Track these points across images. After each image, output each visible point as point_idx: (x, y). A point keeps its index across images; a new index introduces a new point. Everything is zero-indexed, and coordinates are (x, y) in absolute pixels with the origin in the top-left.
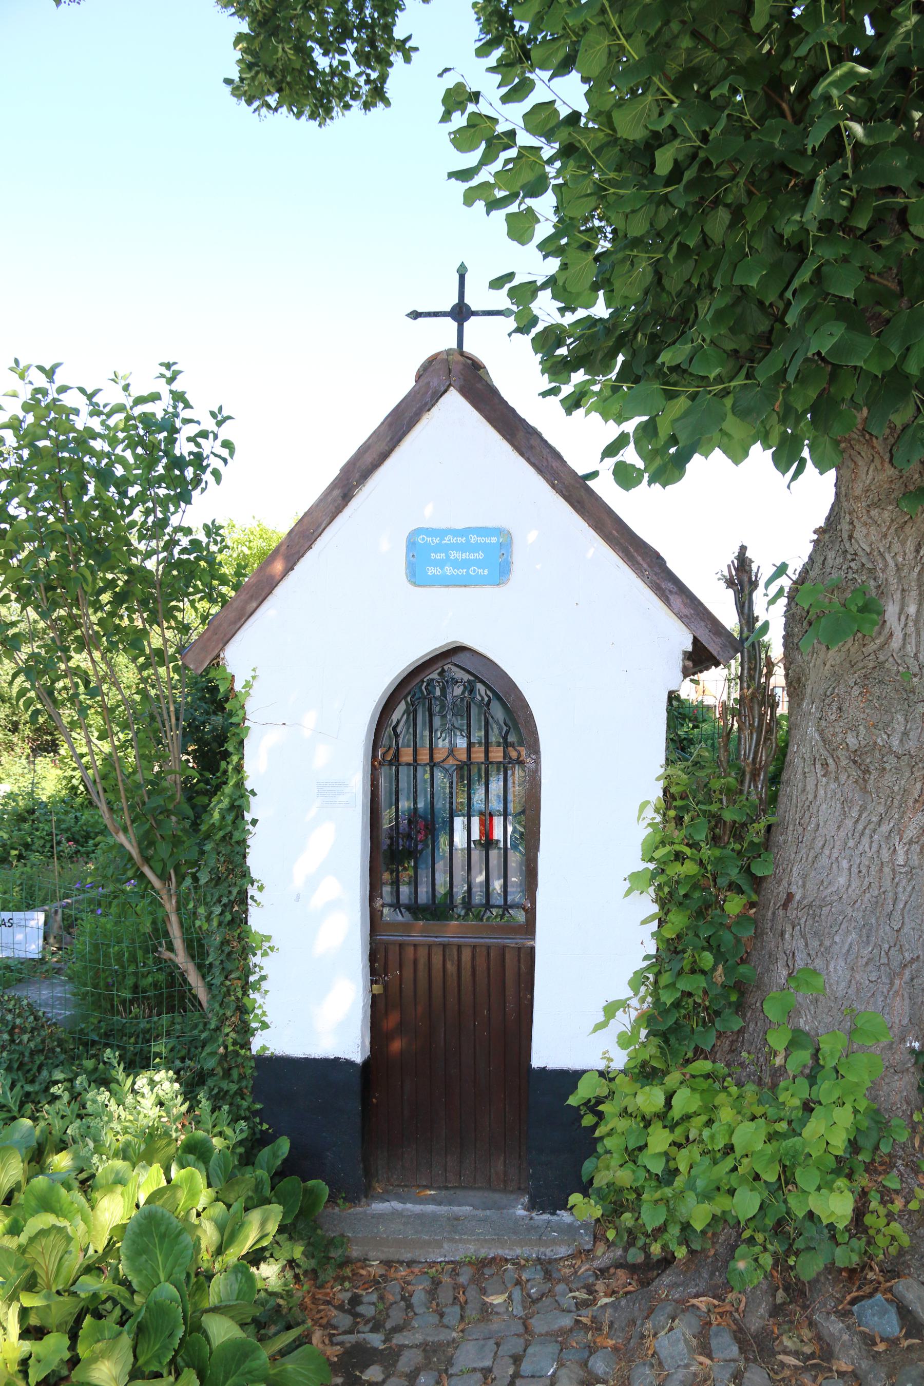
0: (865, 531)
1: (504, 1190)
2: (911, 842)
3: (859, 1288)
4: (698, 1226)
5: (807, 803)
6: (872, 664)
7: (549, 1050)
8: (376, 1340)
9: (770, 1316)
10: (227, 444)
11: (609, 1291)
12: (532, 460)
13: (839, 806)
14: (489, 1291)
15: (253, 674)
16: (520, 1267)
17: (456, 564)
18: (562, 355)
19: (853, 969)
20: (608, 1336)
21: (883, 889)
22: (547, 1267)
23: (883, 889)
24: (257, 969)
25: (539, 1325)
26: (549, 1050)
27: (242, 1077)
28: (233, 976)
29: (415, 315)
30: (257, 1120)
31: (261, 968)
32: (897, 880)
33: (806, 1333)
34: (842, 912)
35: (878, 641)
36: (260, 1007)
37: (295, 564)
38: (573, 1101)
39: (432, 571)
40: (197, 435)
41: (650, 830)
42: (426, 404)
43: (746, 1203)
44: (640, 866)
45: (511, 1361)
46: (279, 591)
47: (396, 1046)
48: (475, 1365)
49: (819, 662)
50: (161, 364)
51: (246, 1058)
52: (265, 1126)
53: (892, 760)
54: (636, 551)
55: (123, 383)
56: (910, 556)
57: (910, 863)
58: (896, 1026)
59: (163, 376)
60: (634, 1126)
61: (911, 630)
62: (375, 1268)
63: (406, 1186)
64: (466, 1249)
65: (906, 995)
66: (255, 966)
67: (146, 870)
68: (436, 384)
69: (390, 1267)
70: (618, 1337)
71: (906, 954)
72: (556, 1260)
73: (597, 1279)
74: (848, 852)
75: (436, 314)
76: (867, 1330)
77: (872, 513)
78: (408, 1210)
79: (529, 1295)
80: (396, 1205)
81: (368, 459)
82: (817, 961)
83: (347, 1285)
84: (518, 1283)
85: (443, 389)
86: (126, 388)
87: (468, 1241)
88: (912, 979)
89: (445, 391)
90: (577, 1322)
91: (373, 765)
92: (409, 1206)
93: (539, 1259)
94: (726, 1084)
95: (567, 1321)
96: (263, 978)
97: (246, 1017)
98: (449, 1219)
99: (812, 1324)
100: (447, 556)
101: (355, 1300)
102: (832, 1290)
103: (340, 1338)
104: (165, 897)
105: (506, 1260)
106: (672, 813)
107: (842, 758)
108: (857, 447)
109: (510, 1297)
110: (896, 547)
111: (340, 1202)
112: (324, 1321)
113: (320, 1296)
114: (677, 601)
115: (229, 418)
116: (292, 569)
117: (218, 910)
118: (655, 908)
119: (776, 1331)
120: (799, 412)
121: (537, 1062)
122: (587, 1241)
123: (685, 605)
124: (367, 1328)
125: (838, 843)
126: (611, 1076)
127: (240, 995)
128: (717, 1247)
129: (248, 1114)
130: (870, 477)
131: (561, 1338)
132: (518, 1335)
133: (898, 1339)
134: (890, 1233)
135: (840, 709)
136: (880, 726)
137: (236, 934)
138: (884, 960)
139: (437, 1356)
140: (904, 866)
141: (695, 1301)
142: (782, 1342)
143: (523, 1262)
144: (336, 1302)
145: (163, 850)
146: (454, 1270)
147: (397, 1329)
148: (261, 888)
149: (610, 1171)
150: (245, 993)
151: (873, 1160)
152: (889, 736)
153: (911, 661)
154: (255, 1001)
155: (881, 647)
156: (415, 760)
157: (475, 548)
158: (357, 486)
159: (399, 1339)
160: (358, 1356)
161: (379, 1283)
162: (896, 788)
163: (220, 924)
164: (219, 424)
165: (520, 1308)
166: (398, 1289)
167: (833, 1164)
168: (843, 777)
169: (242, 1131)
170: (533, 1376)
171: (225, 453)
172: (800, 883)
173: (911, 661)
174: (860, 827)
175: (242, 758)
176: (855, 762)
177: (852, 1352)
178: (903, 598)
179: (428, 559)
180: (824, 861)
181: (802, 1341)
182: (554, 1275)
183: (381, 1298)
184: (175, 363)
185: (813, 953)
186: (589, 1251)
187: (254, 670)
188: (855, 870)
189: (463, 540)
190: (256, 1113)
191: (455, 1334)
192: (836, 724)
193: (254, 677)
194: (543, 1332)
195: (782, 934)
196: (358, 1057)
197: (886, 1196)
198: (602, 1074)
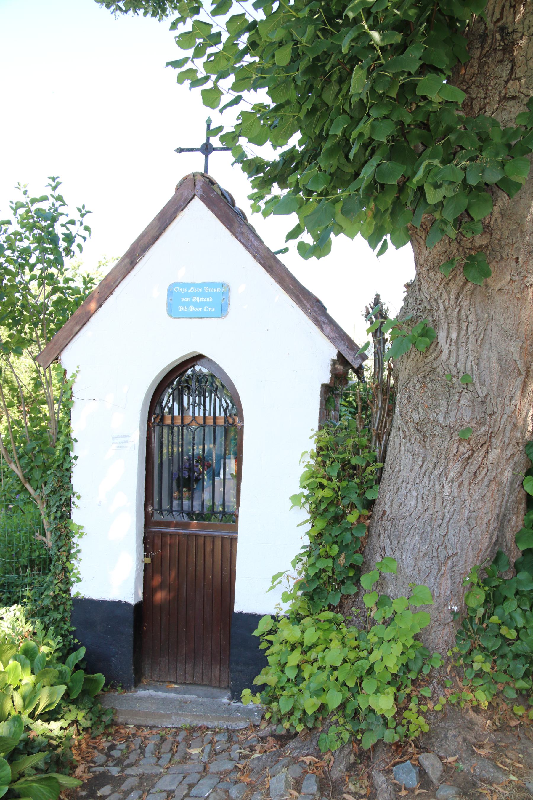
0: (427, 286)
1: (219, 687)
2: (452, 481)
3: (401, 757)
4: (310, 712)
5: (395, 455)
6: (428, 369)
7: (243, 603)
8: (115, 771)
9: (347, 770)
10: (87, 229)
11: (263, 750)
12: (243, 241)
13: (411, 457)
14: (192, 746)
15: (77, 369)
16: (215, 733)
17: (196, 305)
18: (264, 175)
19: (416, 558)
20: (248, 776)
21: (436, 510)
22: (231, 734)
23: (436, 510)
24: (75, 546)
25: (213, 768)
26: (243, 603)
27: (65, 610)
28: (62, 550)
29: (180, 150)
30: (72, 637)
31: (78, 545)
32: (444, 504)
33: (366, 782)
34: (411, 523)
35: (433, 355)
36: (77, 568)
37: (102, 303)
38: (256, 633)
39: (182, 309)
40: (68, 223)
41: (306, 469)
42: (180, 206)
43: (334, 700)
44: (298, 490)
45: (187, 787)
46: (92, 319)
47: (160, 596)
48: (166, 789)
49: (404, 367)
50: (49, 178)
51: (69, 599)
52: (76, 641)
53: (438, 429)
54: (304, 297)
55: (23, 189)
56: (453, 302)
57: (453, 494)
58: (442, 596)
59: (50, 185)
60: (284, 649)
61: (453, 348)
62: (131, 729)
63: (162, 681)
64: (185, 721)
65: (449, 577)
66: (74, 543)
67: (27, 486)
68: (186, 194)
69: (139, 729)
70: (254, 777)
71: (449, 551)
72: (238, 730)
73: (259, 743)
74: (416, 486)
75: (192, 150)
76: (398, 782)
77: (430, 274)
78: (158, 695)
79: (215, 750)
80: (152, 692)
81: (146, 240)
82: (396, 553)
83: (110, 738)
84: (211, 742)
85: (190, 197)
86: (25, 193)
87: (187, 716)
88: (452, 567)
89: (192, 198)
90: (236, 767)
91: (148, 425)
92: (160, 693)
93: (228, 729)
94: (341, 627)
95: (229, 766)
96: (79, 551)
97: (68, 574)
98: (180, 702)
99: (369, 777)
100: (191, 300)
101: (112, 747)
102: (383, 756)
103: (94, 769)
104: (39, 501)
105: (208, 728)
106: (320, 459)
107: (411, 427)
108: (419, 233)
109: (202, 751)
110: (445, 296)
111: (119, 688)
112: (89, 759)
113: (91, 744)
114: (327, 329)
115: (89, 212)
116: (100, 306)
117: (54, 510)
118: (309, 516)
119: (347, 779)
120: (391, 212)
121: (237, 608)
122: (257, 719)
123: (332, 331)
124: (112, 764)
125: (411, 480)
126: (279, 619)
127: (65, 561)
128: (325, 726)
129: (67, 633)
130: (428, 252)
131: (222, 776)
132: (198, 773)
133: (415, 789)
134: (418, 723)
135: (409, 397)
136: (432, 407)
137: (63, 524)
138: (435, 554)
139: (146, 782)
140: (449, 496)
141: (304, 759)
142: (348, 786)
143: (217, 730)
144: (101, 748)
145: (37, 474)
146: (176, 732)
147: (131, 765)
148: (79, 497)
149: (268, 677)
150: (68, 560)
151: (417, 678)
152: (437, 414)
153: (452, 367)
154: (74, 564)
155: (436, 359)
156: (173, 423)
157: (208, 295)
158: (139, 256)
159: (129, 771)
160: (103, 779)
161: (130, 738)
162: (442, 447)
163: (55, 518)
164: (83, 216)
165: (206, 757)
166: (139, 742)
167: (390, 678)
168: (413, 440)
169: (59, 643)
170: (196, 797)
171: (86, 234)
172: (389, 504)
173: (452, 367)
174: (423, 470)
175: (70, 420)
176: (418, 430)
177: (385, 795)
178: (449, 328)
179: (180, 302)
180: (403, 491)
181: (361, 787)
182: (234, 739)
183: (128, 747)
184: (58, 177)
185: (394, 548)
186: (258, 726)
187: (78, 367)
188: (420, 497)
189: (201, 290)
190: (71, 633)
191: (162, 770)
192: (407, 406)
193: (77, 372)
194: (214, 772)
195: (379, 535)
196: (133, 602)
197: (422, 700)
198: (273, 617)
